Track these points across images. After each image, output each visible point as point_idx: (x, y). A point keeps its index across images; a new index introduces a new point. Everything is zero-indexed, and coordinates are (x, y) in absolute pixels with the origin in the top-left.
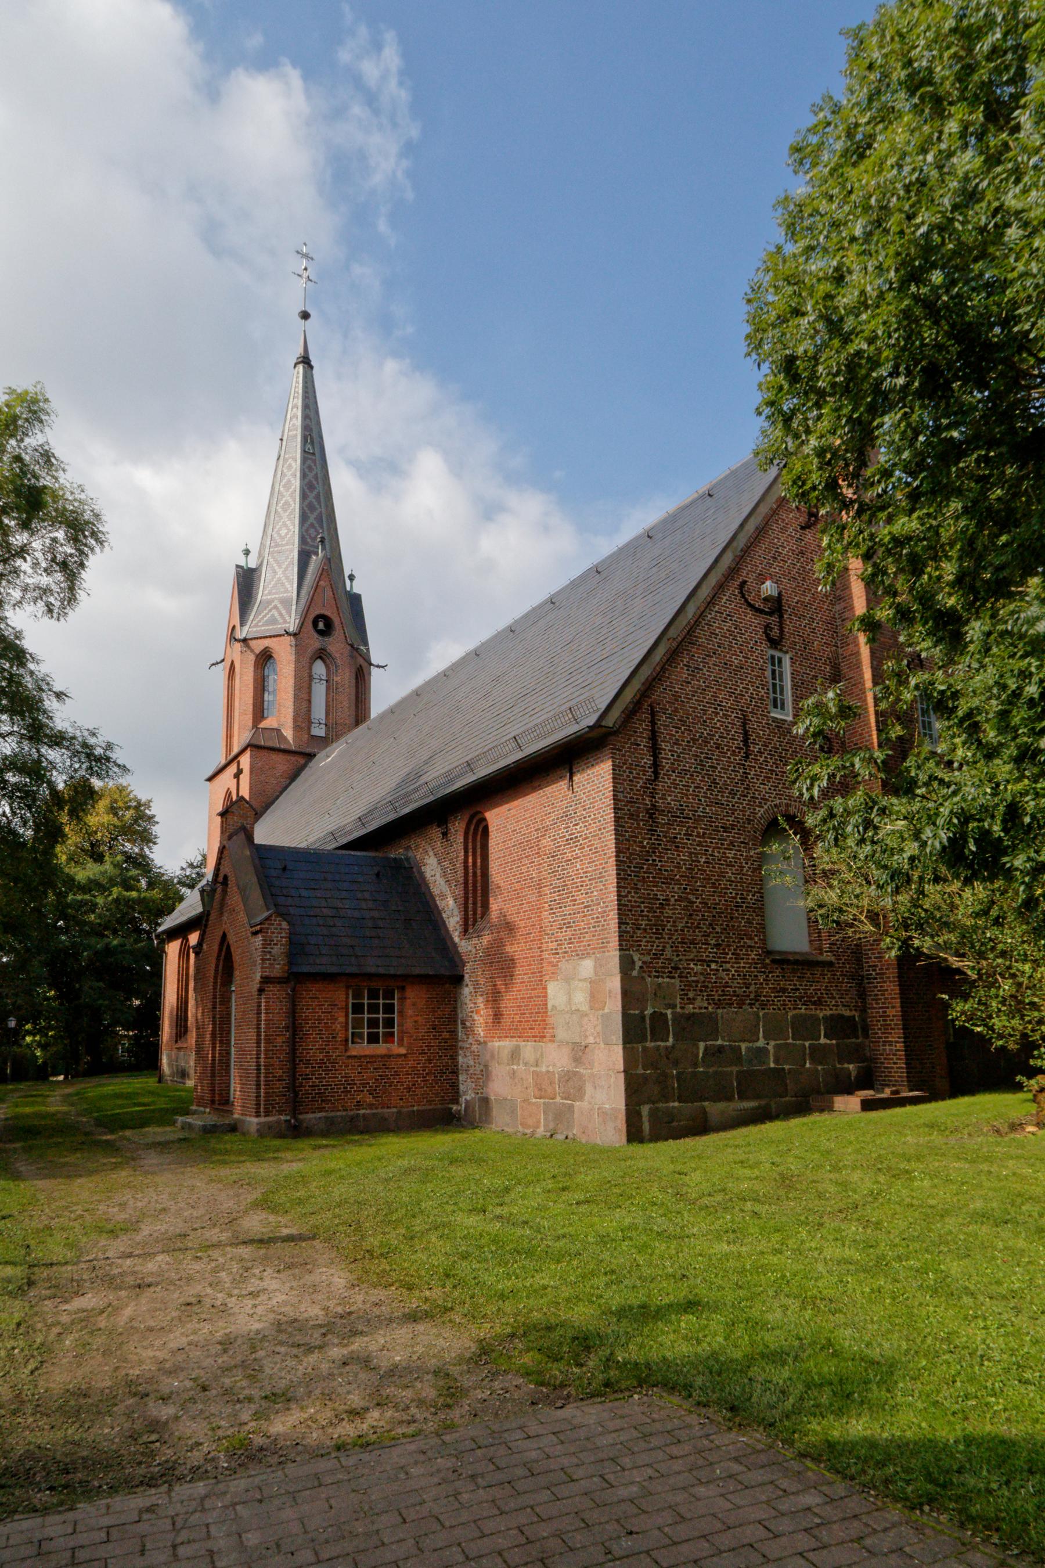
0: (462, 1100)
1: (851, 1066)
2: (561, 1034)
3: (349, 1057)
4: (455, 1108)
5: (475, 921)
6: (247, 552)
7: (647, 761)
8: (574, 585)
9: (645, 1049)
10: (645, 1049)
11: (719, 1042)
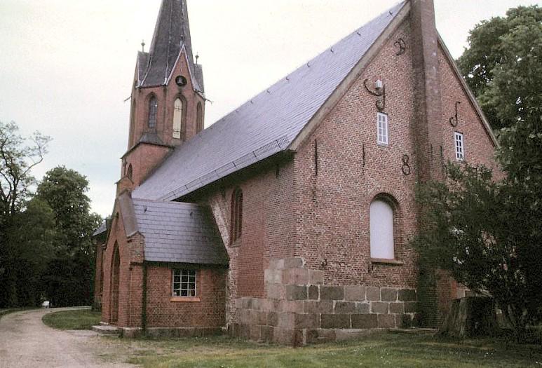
0: (227, 324)
1: (412, 314)
2: (270, 294)
3: (172, 302)
4: (223, 328)
5: (235, 239)
6: (143, 44)
7: (312, 166)
8: (299, 71)
9: (306, 303)
10: (306, 303)
11: (344, 301)
